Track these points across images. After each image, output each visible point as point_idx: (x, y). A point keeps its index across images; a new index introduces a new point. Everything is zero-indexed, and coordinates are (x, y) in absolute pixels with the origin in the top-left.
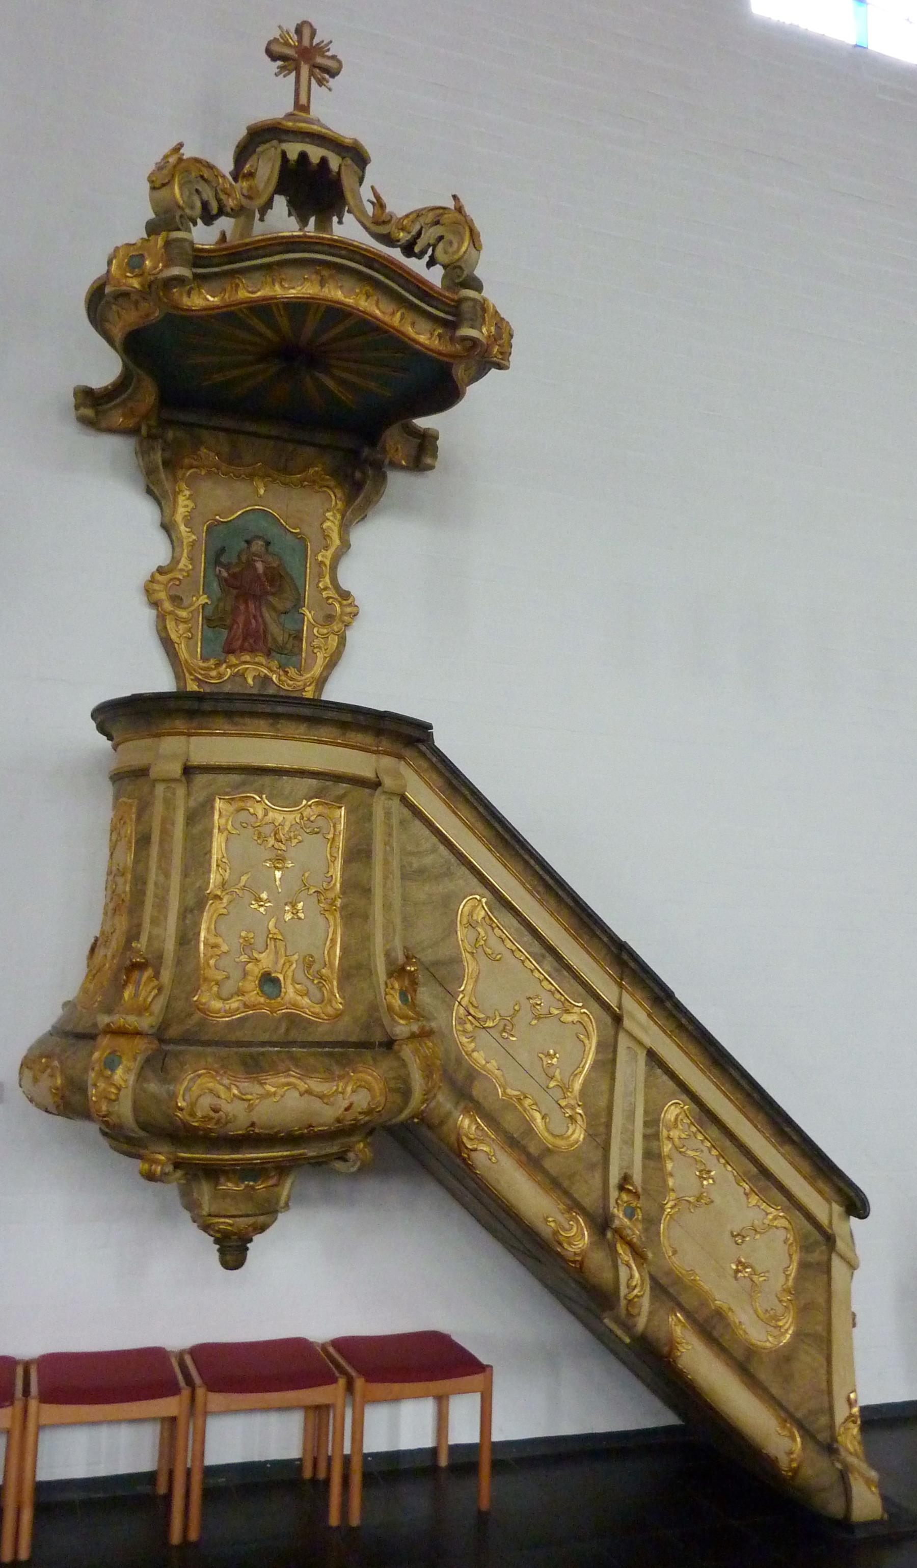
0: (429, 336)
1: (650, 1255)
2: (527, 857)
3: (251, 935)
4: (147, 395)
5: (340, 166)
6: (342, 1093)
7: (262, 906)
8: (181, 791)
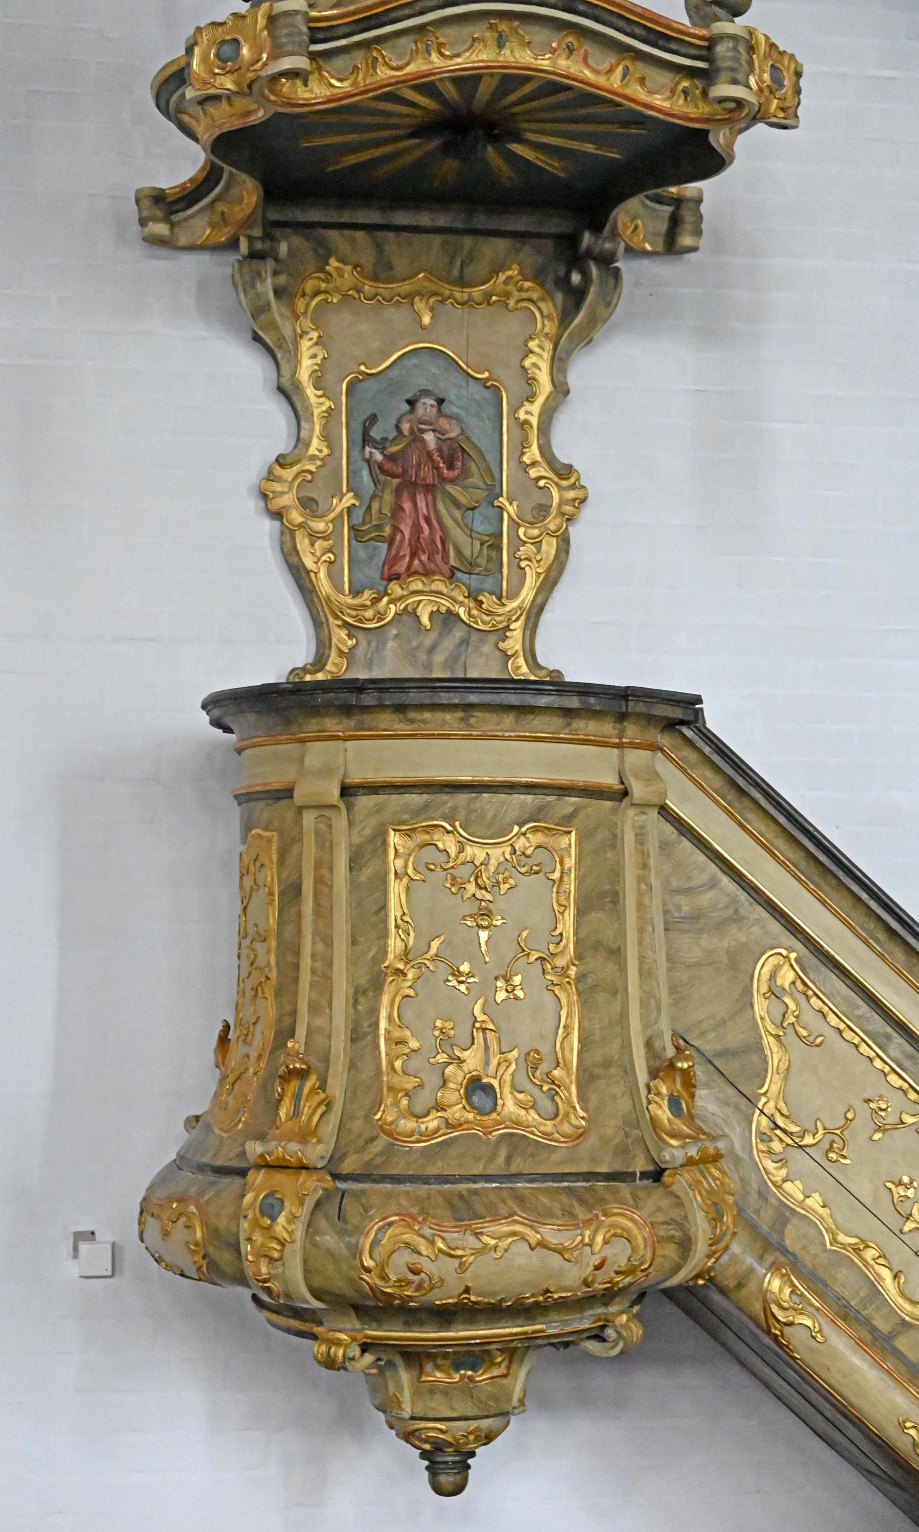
0: (668, 94)
2: (855, 888)
3: (449, 1025)
4: (248, 192)
6: (590, 1245)
7: (462, 982)
8: (341, 821)
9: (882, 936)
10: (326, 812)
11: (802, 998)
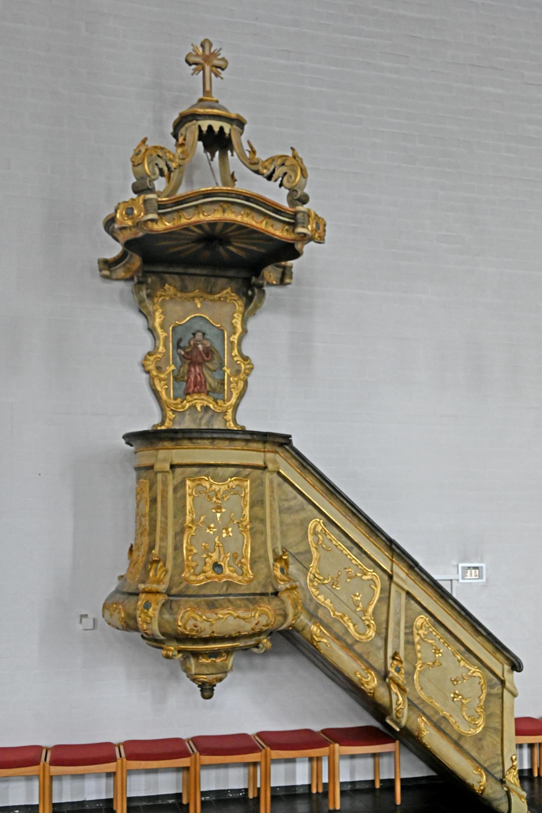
1: (408, 689)
2: (342, 499)
4: (136, 261)
5: (230, 130)
8: (170, 477)
9: (350, 515)
10: (165, 474)
11: (324, 536)
